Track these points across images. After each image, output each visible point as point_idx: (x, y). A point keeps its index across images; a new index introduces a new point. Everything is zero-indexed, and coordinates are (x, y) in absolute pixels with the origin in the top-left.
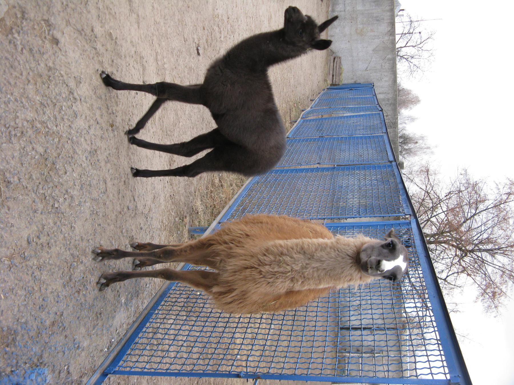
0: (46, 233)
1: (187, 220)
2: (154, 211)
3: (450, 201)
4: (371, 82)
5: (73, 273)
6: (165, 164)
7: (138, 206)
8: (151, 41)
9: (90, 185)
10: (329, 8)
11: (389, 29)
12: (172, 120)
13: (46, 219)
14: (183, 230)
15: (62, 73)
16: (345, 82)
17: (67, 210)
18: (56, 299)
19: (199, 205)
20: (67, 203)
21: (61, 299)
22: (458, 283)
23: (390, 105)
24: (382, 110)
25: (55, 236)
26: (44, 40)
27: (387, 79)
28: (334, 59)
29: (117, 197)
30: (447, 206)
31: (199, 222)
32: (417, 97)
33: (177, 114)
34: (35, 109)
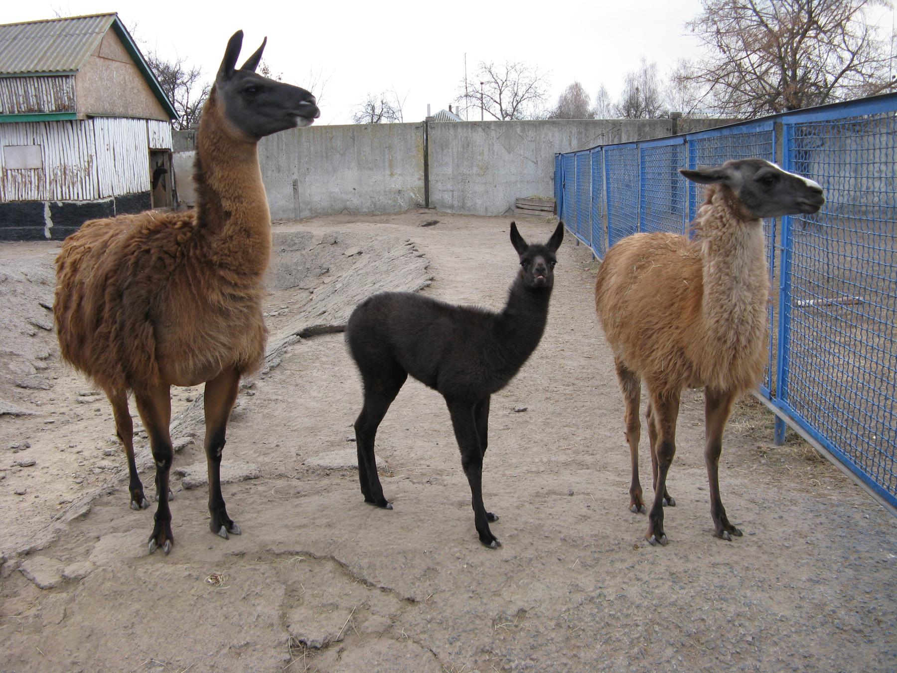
0: (789, 658)
1: (764, 446)
2: (753, 496)
3: (732, 46)
4: (554, 156)
5: (850, 627)
6: (682, 472)
7: (748, 519)
8: (514, 479)
9: (721, 587)
10: (447, 213)
11: (480, 129)
12: (620, 456)
13: (769, 655)
14: (779, 454)
15: (564, 610)
16: (551, 194)
17: (757, 624)
18: (890, 657)
19: (741, 425)
20: (747, 624)
21: (890, 649)
22: (859, 33)
23: (586, 130)
24: (601, 147)
25: (794, 646)
26: (519, 628)
27: (550, 134)
28: (518, 207)
29: (737, 550)
30: (740, 50)
31: (766, 427)
32: (571, 88)
33: (612, 449)
34: (613, 652)
